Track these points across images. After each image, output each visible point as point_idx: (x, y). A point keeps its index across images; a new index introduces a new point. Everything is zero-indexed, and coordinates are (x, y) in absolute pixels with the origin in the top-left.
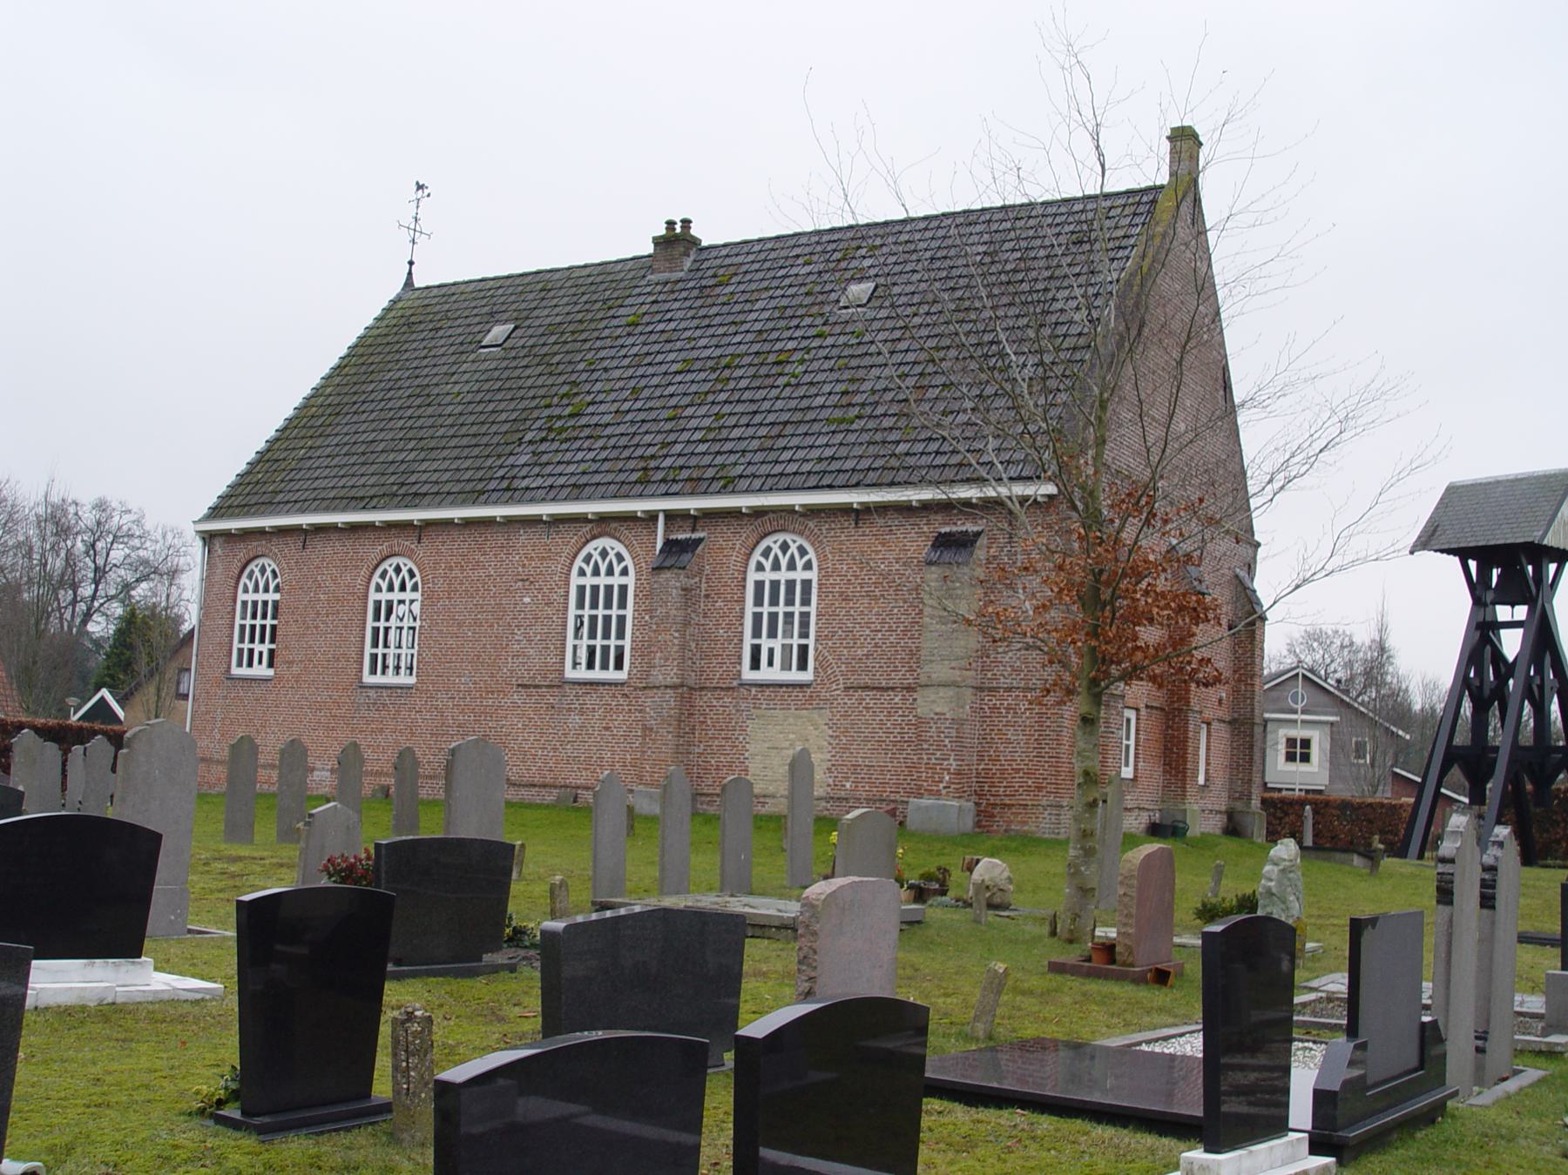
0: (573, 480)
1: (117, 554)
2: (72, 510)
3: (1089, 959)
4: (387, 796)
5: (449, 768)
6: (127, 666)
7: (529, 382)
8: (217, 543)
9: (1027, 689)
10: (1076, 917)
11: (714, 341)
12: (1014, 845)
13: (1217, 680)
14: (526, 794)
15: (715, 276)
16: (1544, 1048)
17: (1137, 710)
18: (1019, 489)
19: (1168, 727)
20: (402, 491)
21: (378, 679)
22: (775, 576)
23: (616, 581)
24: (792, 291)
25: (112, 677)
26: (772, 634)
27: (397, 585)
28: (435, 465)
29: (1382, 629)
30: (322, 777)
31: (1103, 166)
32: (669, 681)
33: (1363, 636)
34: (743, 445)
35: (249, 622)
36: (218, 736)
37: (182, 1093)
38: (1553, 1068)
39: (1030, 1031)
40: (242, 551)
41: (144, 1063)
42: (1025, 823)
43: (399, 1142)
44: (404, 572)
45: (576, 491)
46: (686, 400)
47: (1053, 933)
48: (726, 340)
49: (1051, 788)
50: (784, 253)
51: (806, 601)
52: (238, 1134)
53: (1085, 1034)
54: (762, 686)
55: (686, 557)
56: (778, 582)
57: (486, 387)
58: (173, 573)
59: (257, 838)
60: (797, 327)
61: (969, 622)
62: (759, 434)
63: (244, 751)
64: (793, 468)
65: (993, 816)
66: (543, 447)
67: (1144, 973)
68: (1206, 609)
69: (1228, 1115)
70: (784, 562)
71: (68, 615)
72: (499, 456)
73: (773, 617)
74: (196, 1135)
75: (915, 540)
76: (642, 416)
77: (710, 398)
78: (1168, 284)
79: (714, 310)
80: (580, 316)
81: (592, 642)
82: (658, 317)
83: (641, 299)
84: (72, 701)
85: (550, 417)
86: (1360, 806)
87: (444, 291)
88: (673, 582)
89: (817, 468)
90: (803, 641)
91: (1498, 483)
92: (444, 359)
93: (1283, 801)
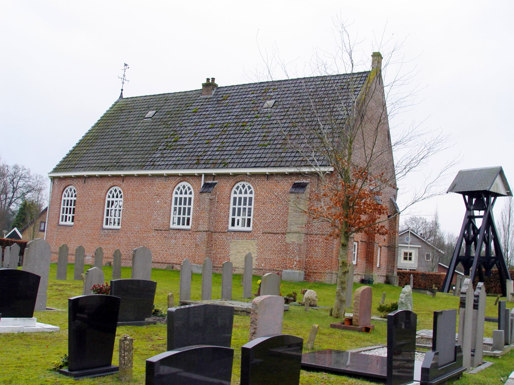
0: (174, 163)
1: (21, 183)
2: (6, 168)
3: (343, 324)
4: (110, 265)
5: (134, 256)
6: (23, 220)
7: (160, 130)
8: (56, 181)
9: (322, 235)
10: (339, 310)
11: (222, 118)
12: (317, 285)
13: (386, 233)
14: (157, 266)
15: (222, 97)
16: (492, 355)
17: (358, 242)
18: (323, 169)
19: (368, 248)
20: (118, 165)
21: (108, 227)
22: (240, 196)
23: (188, 196)
24: (247, 102)
25: (18, 224)
26: (239, 215)
27: (115, 196)
28: (129, 157)
29: (436, 217)
30: (89, 259)
31: (353, 64)
32: (204, 230)
33: (430, 219)
34: (230, 153)
35: (66, 207)
36: (54, 244)
37: (48, 363)
38: (496, 361)
39: (326, 347)
40: (64, 183)
41: (34, 353)
42: (320, 278)
43: (121, 380)
44: (118, 192)
45: (175, 166)
46: (212, 137)
47: (331, 315)
48: (225, 118)
49: (329, 267)
50: (245, 90)
51: (250, 204)
52: (68, 377)
53: (343, 348)
54: (235, 232)
55: (211, 189)
57: (146, 131)
58: (40, 190)
59: (67, 278)
60: (249, 114)
61: (306, 212)
62: (236, 149)
63: (64, 250)
64: (247, 160)
65: (310, 276)
66: (165, 151)
67: (362, 328)
68: (384, 210)
69: (395, 376)
70: (243, 191)
71: (3, 203)
72: (150, 154)
73: (239, 209)
74: (53, 377)
75: (287, 185)
76: (197, 142)
77: (220, 137)
78: (372, 104)
79: (222, 108)
80: (177, 109)
81: (179, 216)
82: (203, 110)
83: (198, 104)
84: (5, 231)
85: (167, 142)
86: (428, 275)
87: (133, 99)
88: (206, 197)
89: (255, 161)
90: (249, 217)
91: (475, 171)
92: (132, 122)
93: (403, 273)
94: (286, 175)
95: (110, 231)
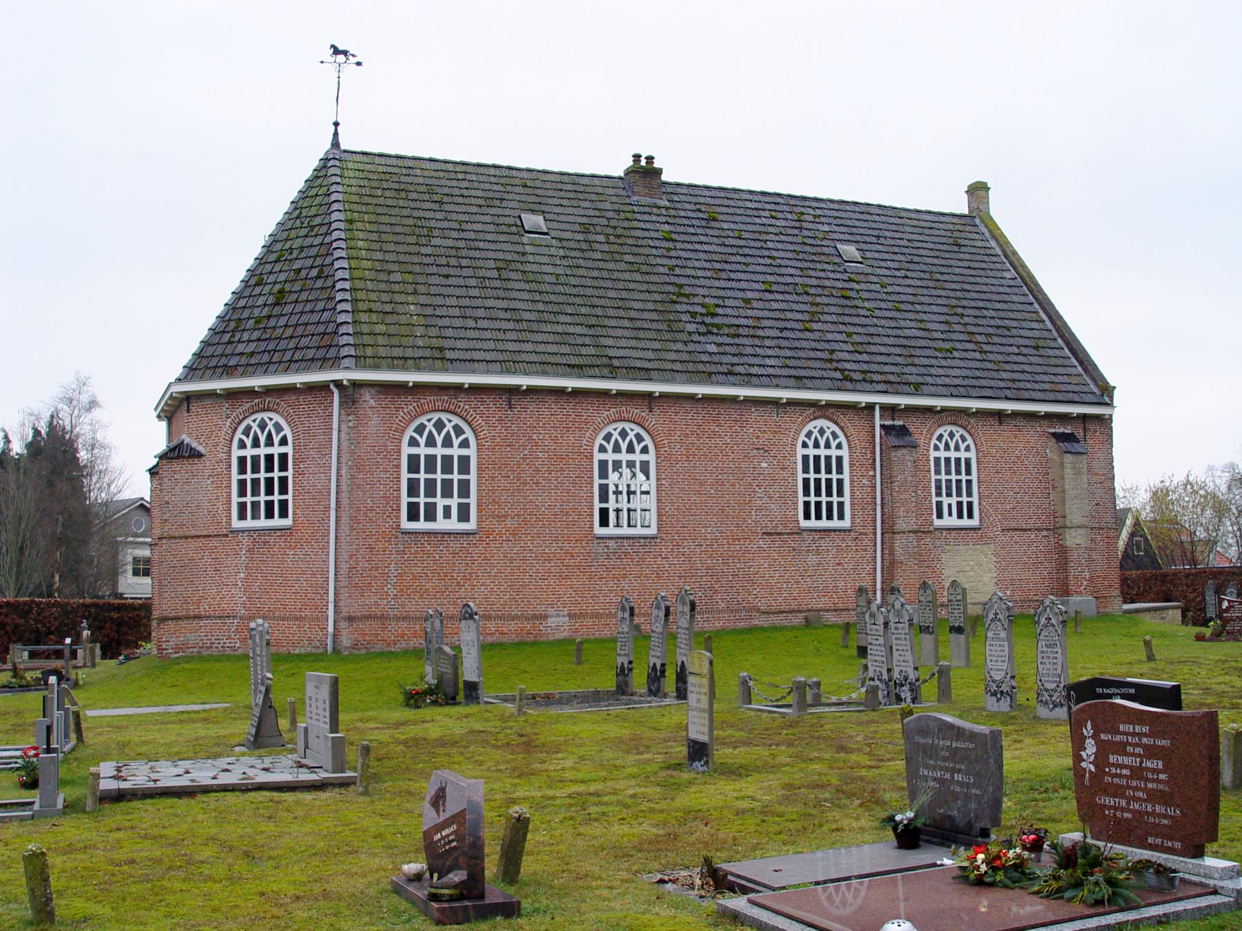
22: (256, 452)
32: (911, 528)
56: (245, 458)
95: (626, 543)
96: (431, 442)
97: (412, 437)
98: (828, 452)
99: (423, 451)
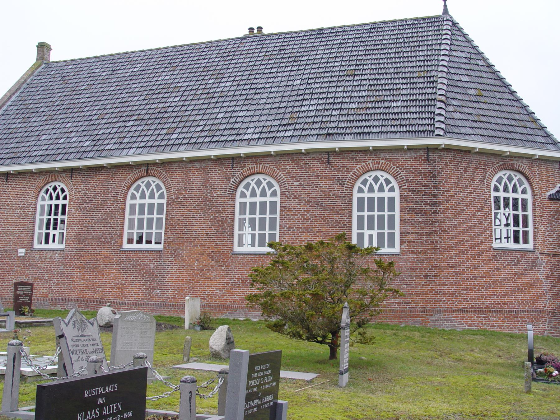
22: (371, 195)
26: (55, 228)
44: (59, 190)
94: (183, 161)
96: (506, 189)
97: (242, 192)
98: (515, 196)
99: (501, 194)
